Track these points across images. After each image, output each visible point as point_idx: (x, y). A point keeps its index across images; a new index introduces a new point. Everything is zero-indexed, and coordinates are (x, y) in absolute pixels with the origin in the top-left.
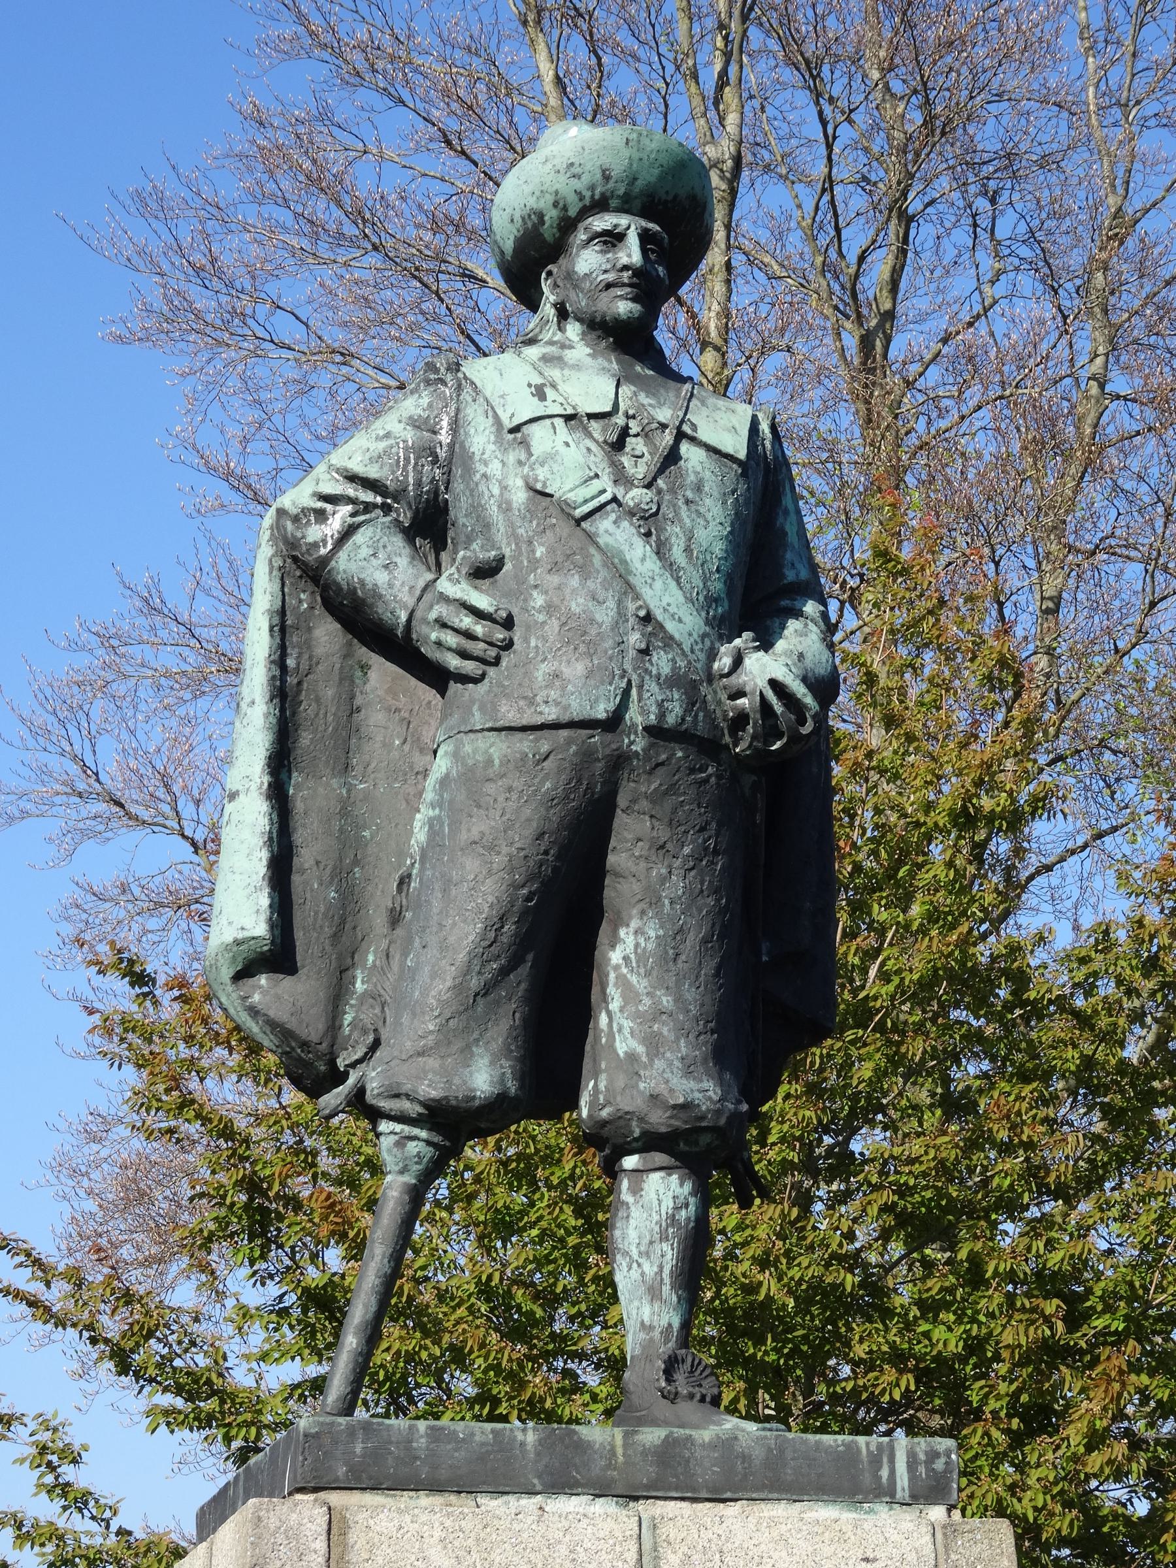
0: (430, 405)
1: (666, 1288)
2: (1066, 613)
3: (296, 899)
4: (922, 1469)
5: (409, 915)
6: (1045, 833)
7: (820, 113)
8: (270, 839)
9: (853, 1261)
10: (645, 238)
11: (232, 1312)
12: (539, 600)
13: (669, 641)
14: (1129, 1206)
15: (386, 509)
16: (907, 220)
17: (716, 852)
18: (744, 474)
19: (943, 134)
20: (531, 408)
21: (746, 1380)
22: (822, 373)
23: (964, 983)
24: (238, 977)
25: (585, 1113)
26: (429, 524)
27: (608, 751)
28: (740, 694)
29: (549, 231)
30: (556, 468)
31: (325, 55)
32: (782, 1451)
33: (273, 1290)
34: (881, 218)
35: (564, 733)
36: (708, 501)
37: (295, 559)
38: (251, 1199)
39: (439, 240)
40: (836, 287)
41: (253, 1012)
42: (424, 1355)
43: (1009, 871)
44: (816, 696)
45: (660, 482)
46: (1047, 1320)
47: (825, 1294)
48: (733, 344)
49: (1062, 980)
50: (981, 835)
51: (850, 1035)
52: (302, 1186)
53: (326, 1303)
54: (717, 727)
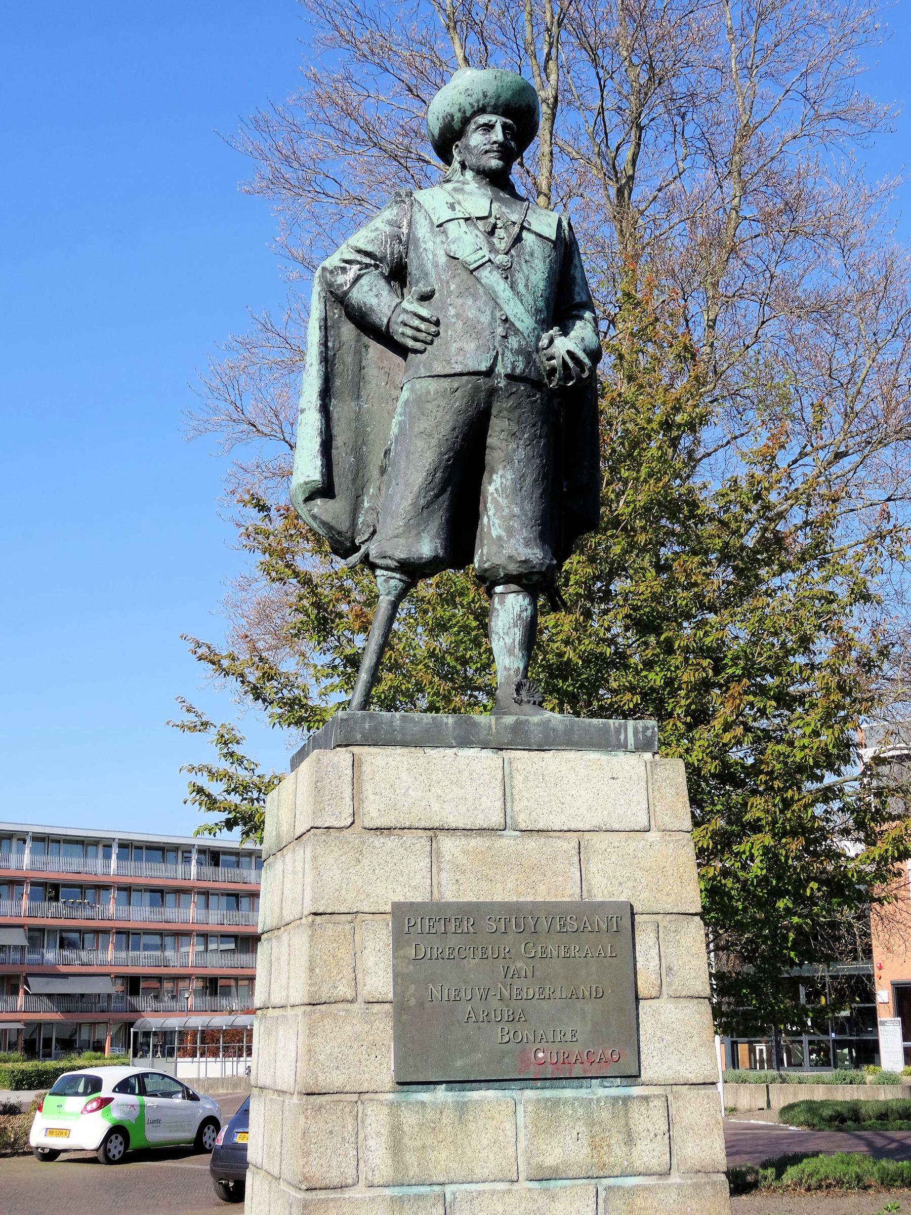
0: (398, 214)
1: (517, 650)
2: (720, 327)
3: (335, 461)
4: (640, 735)
5: (389, 469)
6: (709, 435)
7: (597, 74)
8: (321, 432)
9: (612, 642)
10: (505, 127)
11: (307, 667)
12: (452, 311)
13: (517, 332)
14: (745, 615)
15: (376, 267)
16: (640, 128)
17: (540, 437)
18: (555, 247)
19: (660, 83)
20: (450, 214)
21: (558, 699)
22: (599, 207)
23: (666, 507)
24: (306, 500)
25: (477, 566)
26: (398, 274)
27: (487, 387)
28: (552, 358)
29: (456, 124)
30: (460, 244)
31: (348, 46)
32: (572, 726)
33: (328, 658)
34: (627, 128)
35: (465, 378)
36: (536, 261)
37: (331, 292)
38: (319, 613)
39: (406, 141)
40: (604, 164)
41: (314, 517)
42: (403, 687)
43: (690, 453)
44: (590, 359)
45: (512, 251)
46: (704, 669)
47: (597, 658)
48: (554, 192)
49: (714, 507)
50: (675, 433)
51: (609, 533)
52: (343, 607)
53: (354, 661)
54: (541, 374)
